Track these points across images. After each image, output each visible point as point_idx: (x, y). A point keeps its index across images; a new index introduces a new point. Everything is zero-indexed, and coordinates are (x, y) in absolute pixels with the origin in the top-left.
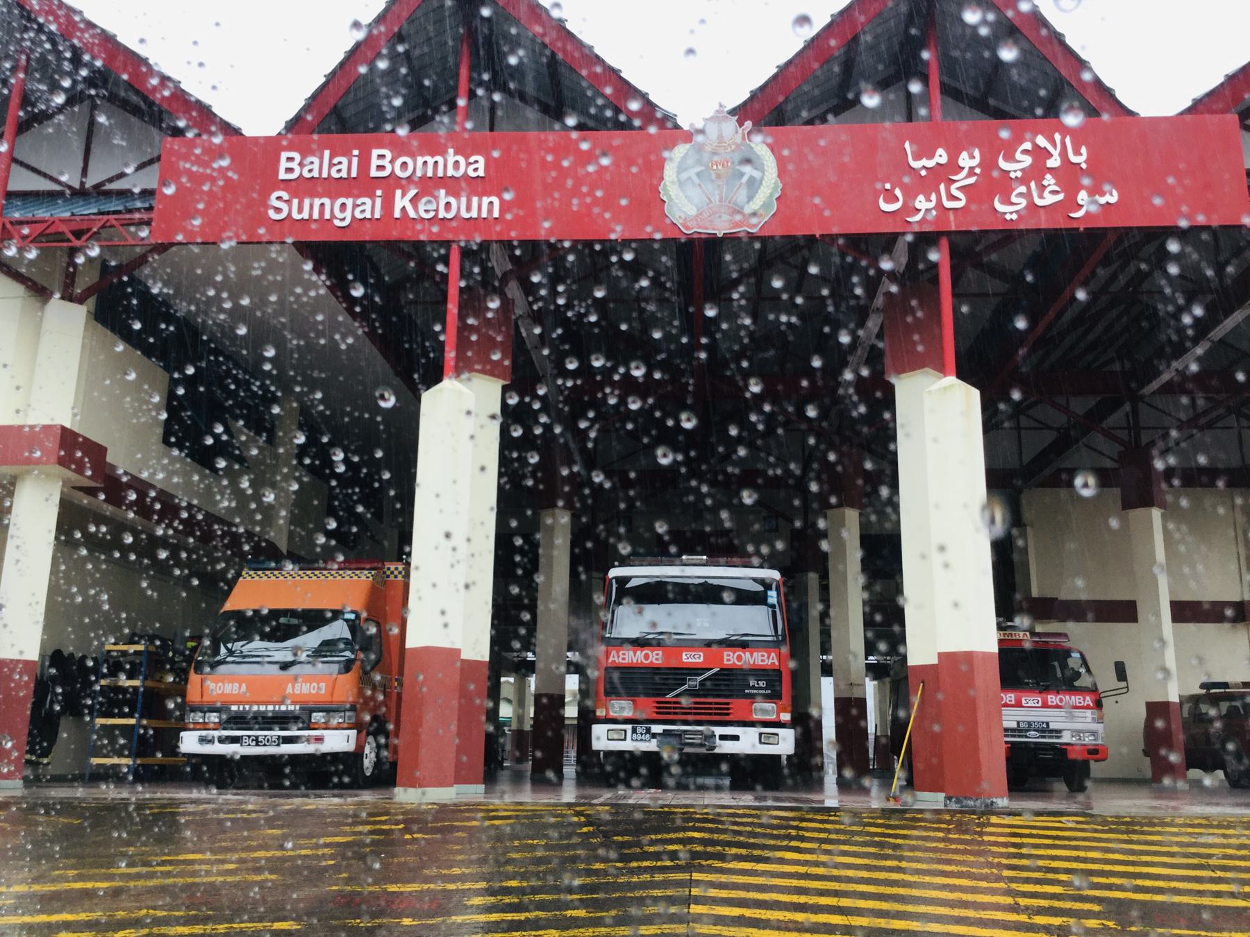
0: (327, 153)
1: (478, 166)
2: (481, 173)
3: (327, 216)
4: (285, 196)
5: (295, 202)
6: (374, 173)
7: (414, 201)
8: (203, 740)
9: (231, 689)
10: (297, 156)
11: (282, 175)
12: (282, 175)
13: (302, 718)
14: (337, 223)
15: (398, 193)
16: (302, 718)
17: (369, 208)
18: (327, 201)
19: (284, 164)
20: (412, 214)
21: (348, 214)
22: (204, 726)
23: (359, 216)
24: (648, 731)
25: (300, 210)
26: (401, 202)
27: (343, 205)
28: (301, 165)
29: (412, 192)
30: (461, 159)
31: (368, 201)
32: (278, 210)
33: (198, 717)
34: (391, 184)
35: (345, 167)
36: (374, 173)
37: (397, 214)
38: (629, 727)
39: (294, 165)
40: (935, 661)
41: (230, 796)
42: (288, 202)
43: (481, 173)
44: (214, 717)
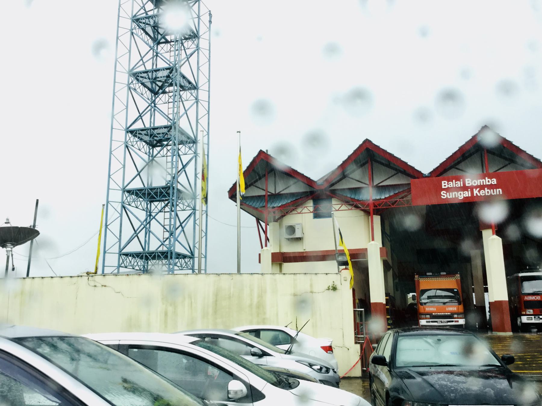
0: (454, 181)
1: (494, 181)
2: (495, 183)
3: (448, 194)
4: (445, 192)
5: (448, 194)
6: (467, 185)
7: (479, 191)
8: (427, 322)
9: (432, 309)
10: (446, 182)
11: (443, 187)
12: (443, 187)
13: (451, 317)
14: (460, 198)
15: (474, 190)
16: (451, 317)
17: (467, 194)
18: (456, 193)
19: (443, 184)
20: (479, 195)
21: (462, 196)
22: (426, 318)
23: (465, 196)
24: (539, 317)
25: (450, 196)
26: (476, 192)
27: (461, 194)
28: (448, 184)
29: (478, 189)
30: (489, 180)
31: (467, 192)
32: (444, 196)
33: (423, 316)
34: (472, 188)
35: (459, 184)
36: (467, 185)
37: (475, 195)
38: (533, 317)
39: (446, 184)
40: (358, 346)
41: (176, 389)
42: (446, 194)
43: (495, 183)
44: (428, 316)
